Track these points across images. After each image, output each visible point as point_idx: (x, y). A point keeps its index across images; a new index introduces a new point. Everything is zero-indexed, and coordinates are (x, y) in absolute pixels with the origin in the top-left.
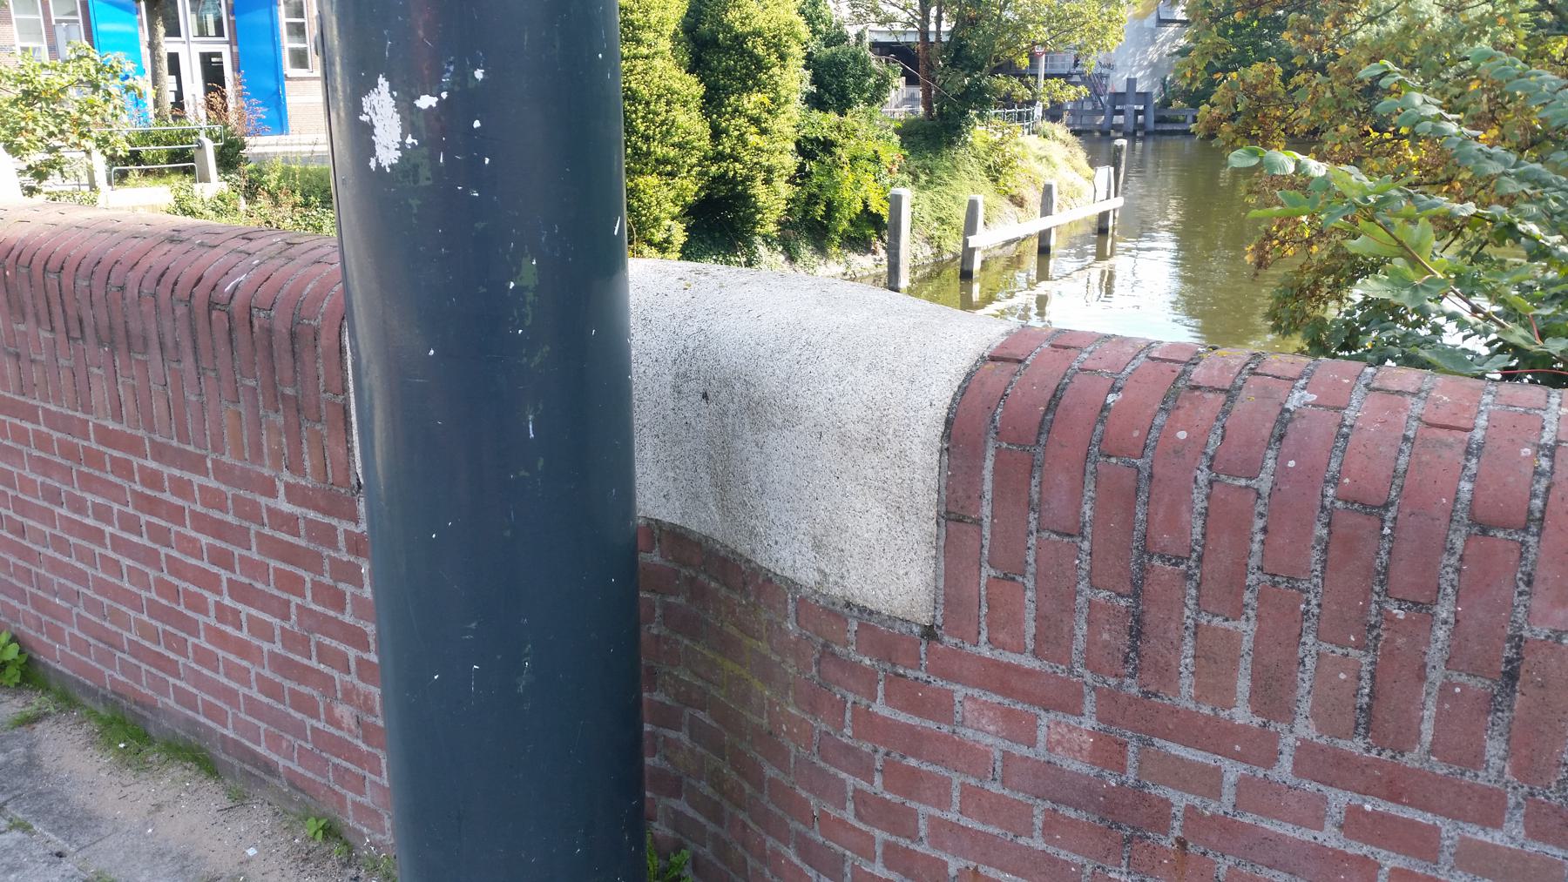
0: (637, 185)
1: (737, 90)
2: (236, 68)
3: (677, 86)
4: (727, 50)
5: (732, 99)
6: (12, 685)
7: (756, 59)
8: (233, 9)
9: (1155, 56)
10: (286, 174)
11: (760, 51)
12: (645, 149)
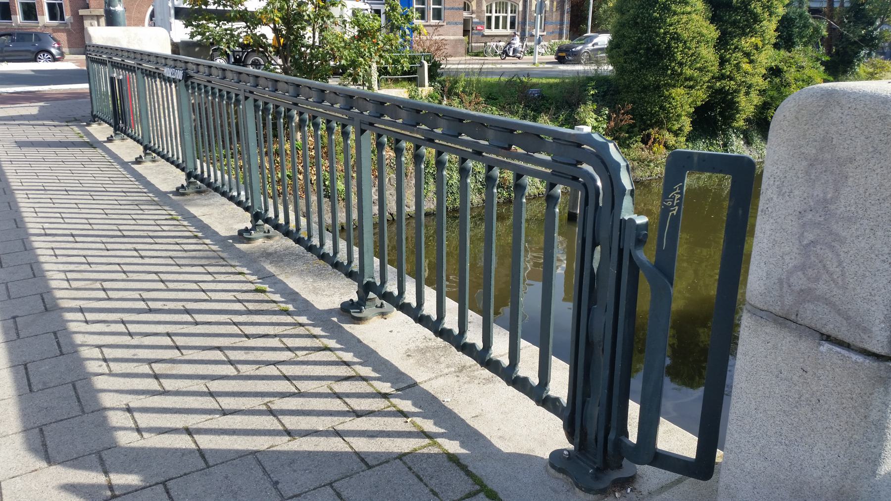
0: (670, 94)
1: (738, 34)
3: (705, 31)
4: (736, 9)
5: (735, 40)
10: (469, 83)
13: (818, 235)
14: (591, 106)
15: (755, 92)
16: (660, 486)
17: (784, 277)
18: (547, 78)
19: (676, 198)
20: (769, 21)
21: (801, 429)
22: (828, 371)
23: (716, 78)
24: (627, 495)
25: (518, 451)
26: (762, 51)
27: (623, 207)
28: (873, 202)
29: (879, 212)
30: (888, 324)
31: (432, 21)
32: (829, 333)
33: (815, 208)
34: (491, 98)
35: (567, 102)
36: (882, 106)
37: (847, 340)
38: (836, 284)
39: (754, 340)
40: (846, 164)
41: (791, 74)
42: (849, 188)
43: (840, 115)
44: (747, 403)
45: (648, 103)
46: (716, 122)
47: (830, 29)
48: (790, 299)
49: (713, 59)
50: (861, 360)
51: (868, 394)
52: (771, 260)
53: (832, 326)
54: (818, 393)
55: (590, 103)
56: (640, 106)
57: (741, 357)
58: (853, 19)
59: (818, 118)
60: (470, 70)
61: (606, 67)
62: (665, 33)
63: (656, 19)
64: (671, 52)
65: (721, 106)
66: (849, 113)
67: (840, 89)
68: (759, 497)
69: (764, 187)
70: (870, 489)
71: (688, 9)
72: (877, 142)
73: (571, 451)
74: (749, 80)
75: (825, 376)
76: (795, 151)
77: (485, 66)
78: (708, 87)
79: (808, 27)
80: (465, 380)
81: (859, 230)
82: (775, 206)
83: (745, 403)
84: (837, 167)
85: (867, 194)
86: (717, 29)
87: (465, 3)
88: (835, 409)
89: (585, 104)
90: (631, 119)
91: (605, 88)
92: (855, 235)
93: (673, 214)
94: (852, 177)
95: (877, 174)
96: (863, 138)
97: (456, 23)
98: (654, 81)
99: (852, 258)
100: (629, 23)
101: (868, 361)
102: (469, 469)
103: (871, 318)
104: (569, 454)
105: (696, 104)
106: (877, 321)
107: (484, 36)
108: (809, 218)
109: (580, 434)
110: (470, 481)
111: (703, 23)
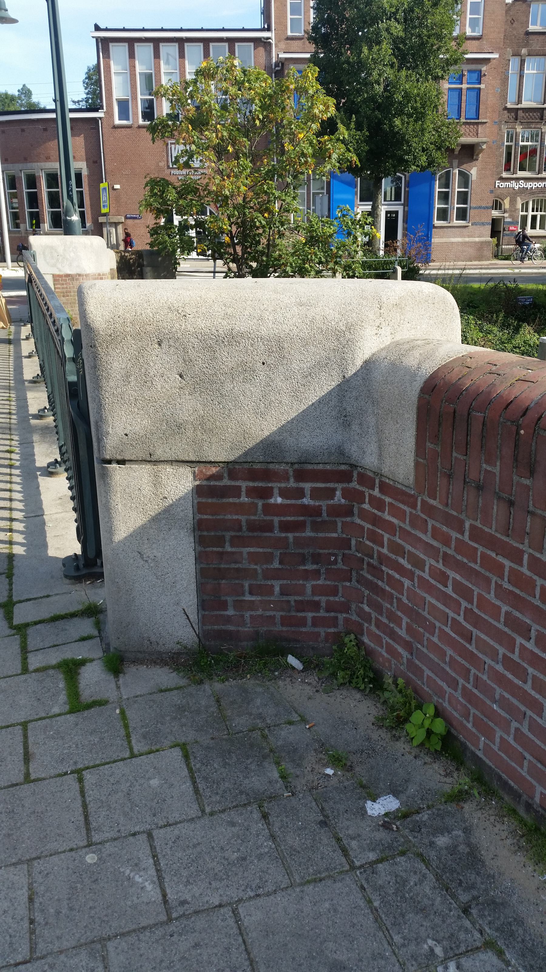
2: (405, 221)
6: (432, 750)
8: (409, 183)
31: (455, 221)
77: (464, 272)
97: (483, 224)
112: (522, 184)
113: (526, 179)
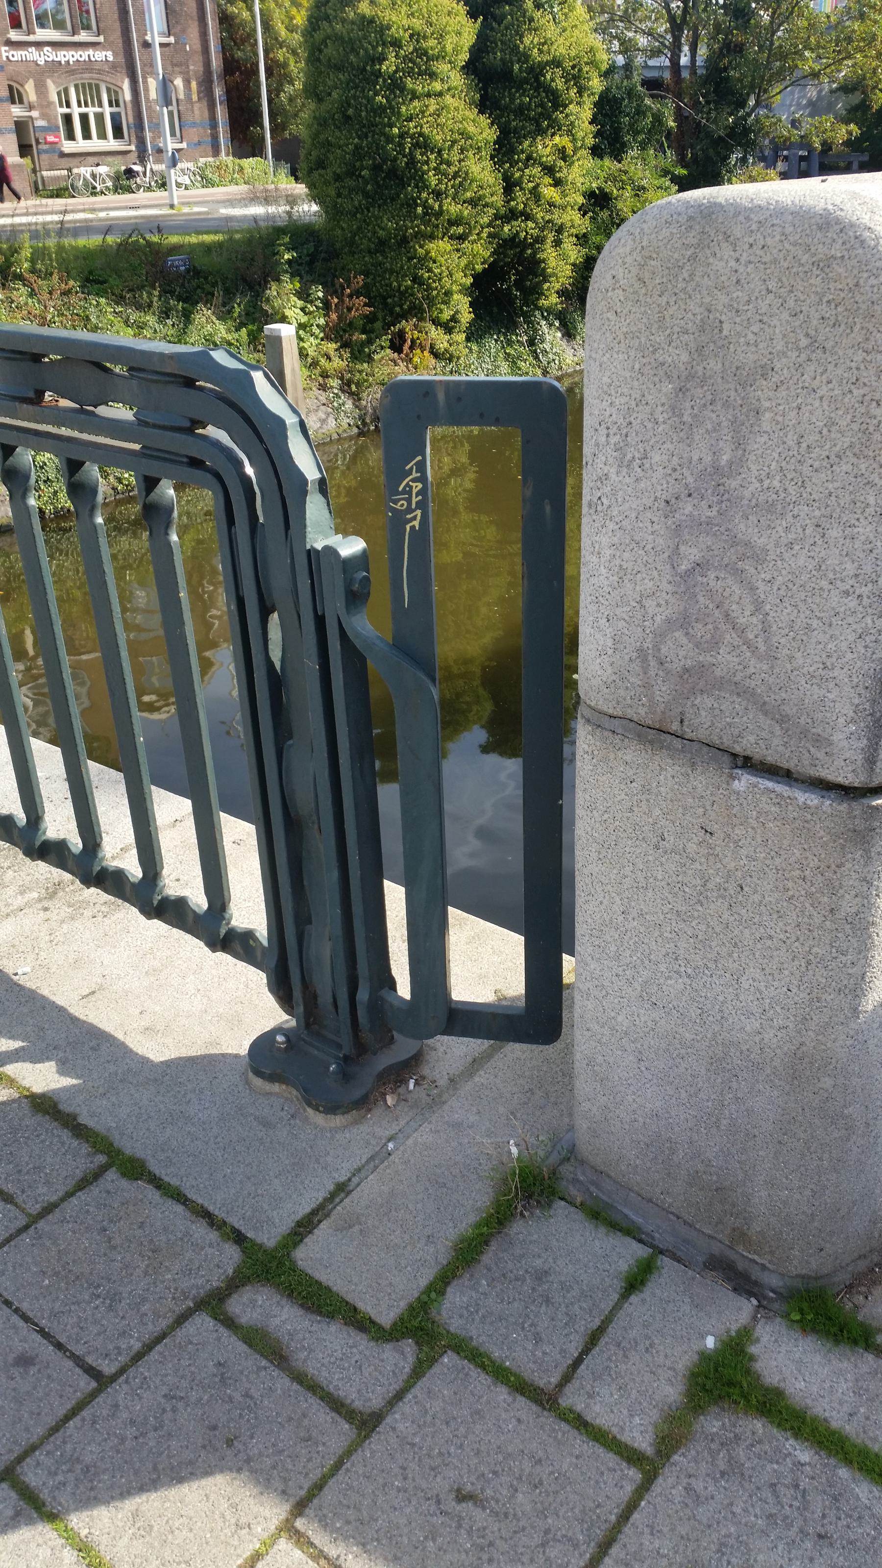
0: (428, 252)
1: (529, 133)
3: (471, 129)
4: (520, 84)
5: (526, 143)
7: (553, 94)
9: (815, 93)
10: (38, 255)
11: (559, 84)
12: (436, 207)
13: (709, 549)
14: (289, 285)
15: (571, 239)
16: (469, 1059)
17: (648, 644)
18: (198, 233)
19: (414, 491)
20: (578, 103)
21: (714, 944)
22: (753, 828)
23: (501, 218)
24: (409, 1096)
25: (185, 1052)
26: (573, 162)
27: (308, 522)
28: (816, 464)
29: (830, 486)
30: (862, 724)
32: (748, 753)
33: (697, 489)
34: (93, 281)
35: (244, 280)
36: (819, 235)
37: (785, 765)
38: (754, 650)
39: (605, 778)
40: (755, 380)
41: (625, 201)
42: (766, 436)
43: (732, 263)
44: (605, 902)
45: (392, 272)
46: (511, 301)
47: (679, 115)
48: (664, 689)
49: (492, 181)
50: (816, 802)
51: (833, 866)
52: (618, 611)
53: (752, 739)
54: (739, 873)
55: (286, 278)
56: (378, 279)
57: (584, 813)
58: (712, 97)
59: (686, 275)
60: (39, 227)
61: (306, 207)
62: (402, 136)
63: (381, 107)
64: (416, 171)
65: (516, 269)
66: (752, 258)
67: (726, 200)
68: (650, 1077)
69: (588, 449)
70: (849, 1042)
71: (437, 86)
72: (815, 322)
73: (291, 1030)
74: (558, 217)
75: (749, 839)
76: (645, 361)
77: (69, 217)
78: (490, 235)
79: (644, 114)
80: (63, 914)
81: (793, 529)
82: (614, 492)
83: (601, 903)
84: (736, 391)
85: (804, 445)
86: (492, 124)
87: (10, 88)
88: (774, 901)
89: (278, 280)
90: (365, 305)
91: (311, 247)
92: (784, 541)
93: (413, 528)
94: (769, 409)
95: (821, 398)
96: (785, 316)
98: (395, 229)
99: (782, 592)
100: (333, 119)
101: (828, 802)
102: (81, 1120)
103: (829, 715)
104: (288, 1040)
105: (474, 269)
106: (841, 720)
107: (63, 155)
108: (687, 512)
109: (304, 998)
110: (85, 1149)
111: (467, 113)
112: (49, 54)
113: (56, 45)
